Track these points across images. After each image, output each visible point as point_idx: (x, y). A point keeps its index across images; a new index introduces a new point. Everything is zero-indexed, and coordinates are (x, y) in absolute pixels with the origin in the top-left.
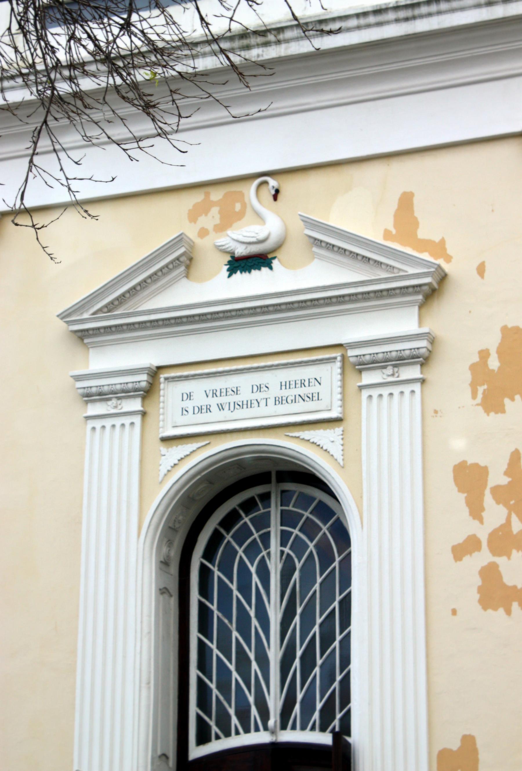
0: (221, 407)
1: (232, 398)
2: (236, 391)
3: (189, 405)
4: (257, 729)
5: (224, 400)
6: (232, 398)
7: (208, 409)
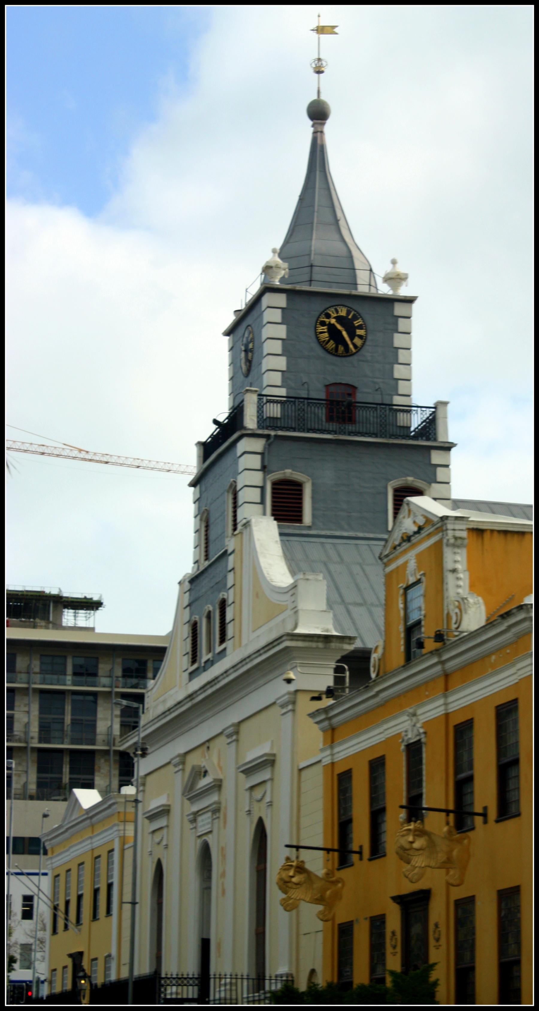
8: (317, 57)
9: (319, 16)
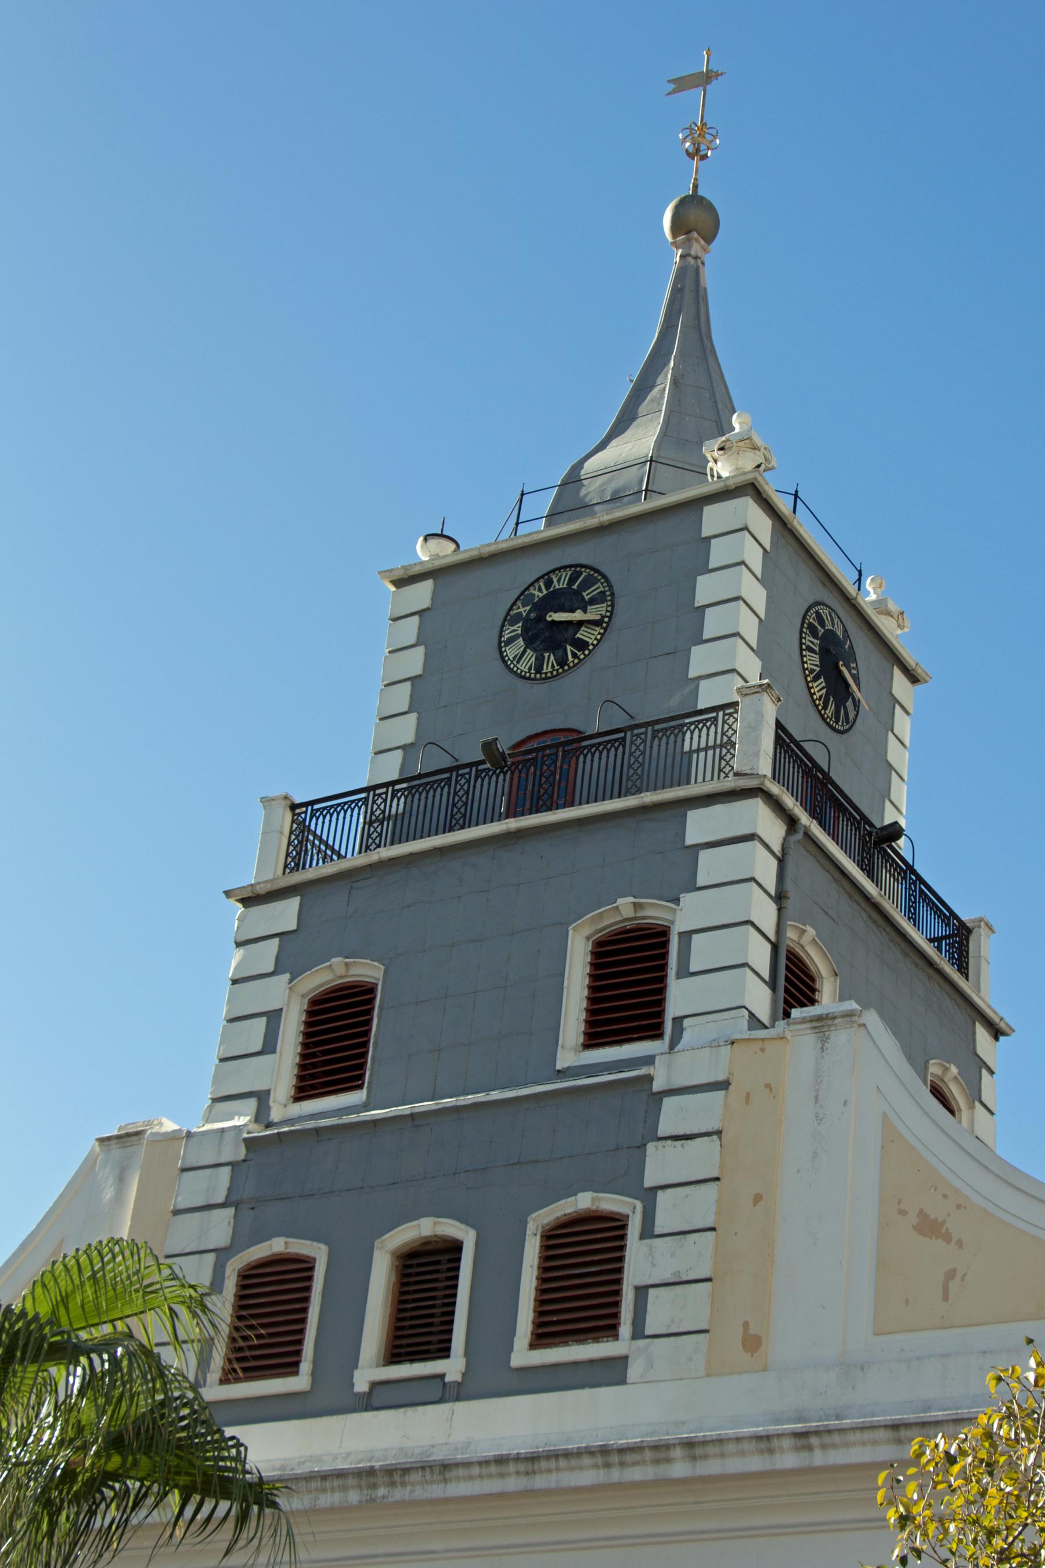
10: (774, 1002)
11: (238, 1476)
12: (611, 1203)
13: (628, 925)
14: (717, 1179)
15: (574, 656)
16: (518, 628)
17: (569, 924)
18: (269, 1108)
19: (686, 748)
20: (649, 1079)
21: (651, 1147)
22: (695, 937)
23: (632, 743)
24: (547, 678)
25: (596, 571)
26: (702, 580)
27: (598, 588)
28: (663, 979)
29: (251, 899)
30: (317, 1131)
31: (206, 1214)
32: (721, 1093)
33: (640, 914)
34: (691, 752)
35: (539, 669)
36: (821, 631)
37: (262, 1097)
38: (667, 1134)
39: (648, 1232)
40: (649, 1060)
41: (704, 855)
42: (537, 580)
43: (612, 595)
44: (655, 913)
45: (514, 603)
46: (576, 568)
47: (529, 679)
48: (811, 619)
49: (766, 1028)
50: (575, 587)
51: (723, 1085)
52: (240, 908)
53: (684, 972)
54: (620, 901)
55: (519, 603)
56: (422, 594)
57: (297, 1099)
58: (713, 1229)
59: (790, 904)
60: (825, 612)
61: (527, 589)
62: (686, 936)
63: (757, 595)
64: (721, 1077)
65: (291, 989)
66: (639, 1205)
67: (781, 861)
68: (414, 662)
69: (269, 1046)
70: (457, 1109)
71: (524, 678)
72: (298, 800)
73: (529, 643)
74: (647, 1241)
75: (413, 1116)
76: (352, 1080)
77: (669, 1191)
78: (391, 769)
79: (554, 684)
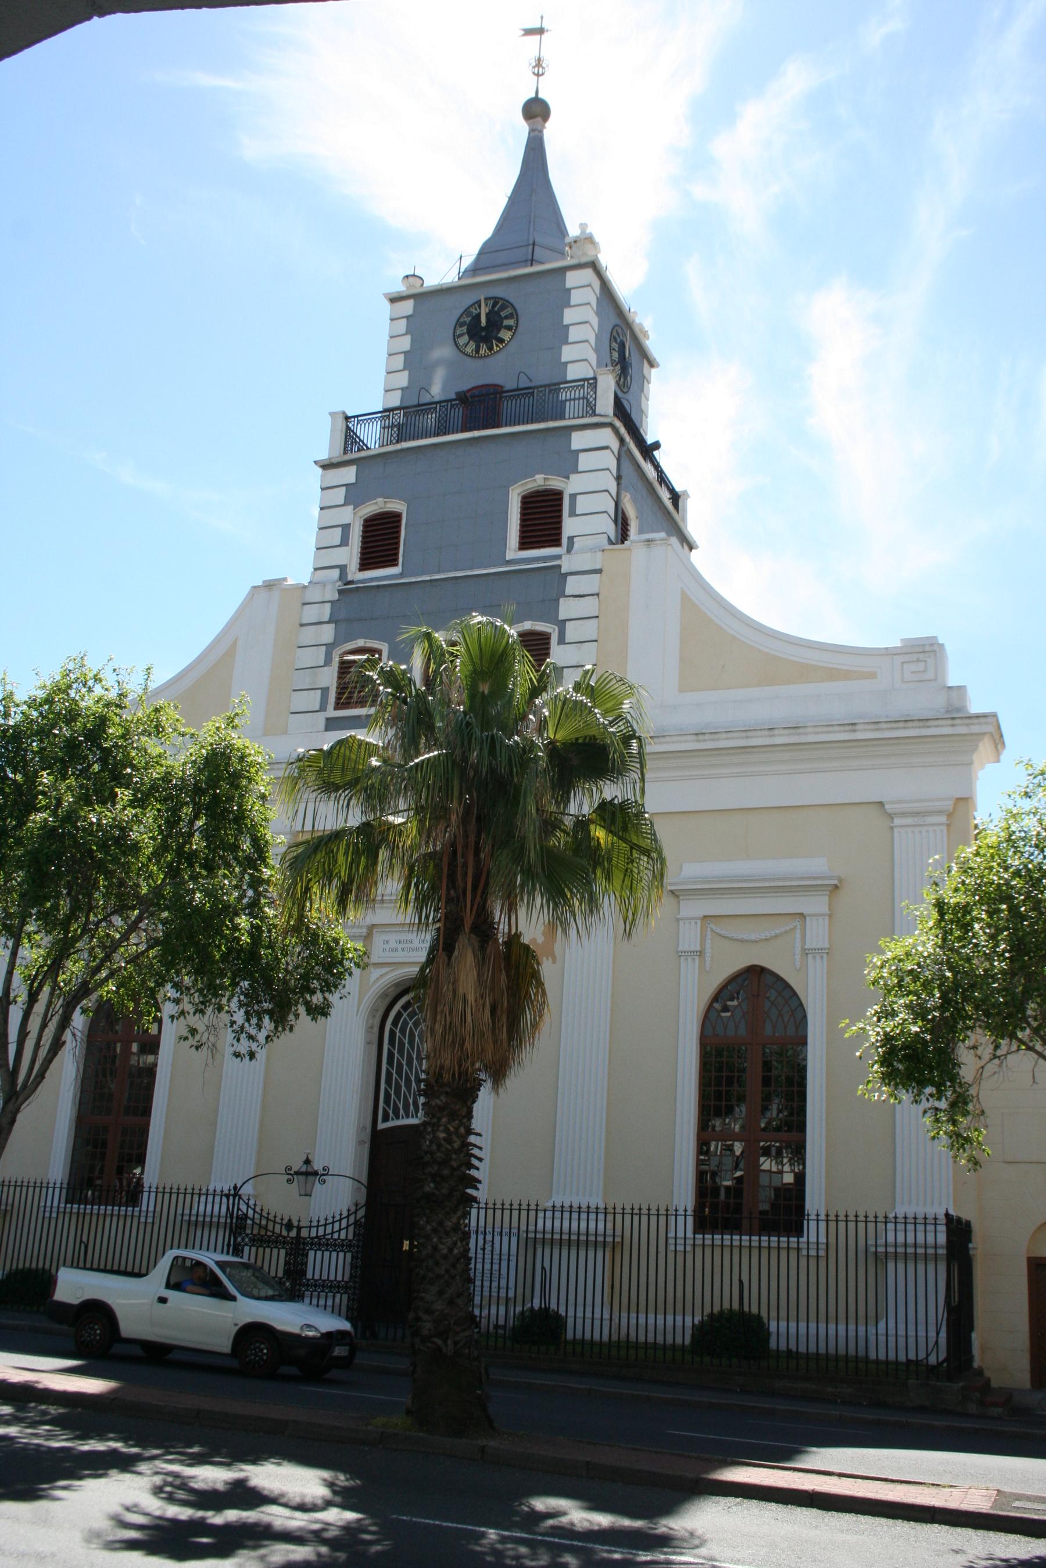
0: (403, 949)
1: (409, 945)
2: (411, 942)
3: (387, 946)
4: (413, 1117)
5: (405, 946)
6: (409, 945)
7: (396, 950)
8: (540, 78)
9: (542, 18)
10: (617, 531)
11: (1033, 1005)
12: (541, 627)
13: (540, 488)
14: (597, 617)
15: (497, 346)
16: (464, 329)
17: (509, 487)
18: (347, 574)
19: (564, 398)
20: (560, 567)
21: (562, 600)
22: (578, 496)
23: (538, 395)
24: (481, 357)
25: (507, 301)
26: (404, 383)
27: (509, 310)
28: (560, 517)
29: (326, 466)
30: (378, 587)
31: (319, 626)
32: (598, 575)
33: (547, 483)
34: (566, 400)
35: (477, 351)
36: (618, 340)
37: (343, 569)
38: (570, 594)
39: (562, 641)
40: (559, 557)
41: (581, 456)
42: (474, 304)
43: (517, 315)
44: (555, 483)
45: (461, 315)
46: (496, 300)
47: (472, 356)
48: (615, 333)
49: (614, 544)
50: (496, 309)
51: (599, 571)
52: (320, 471)
53: (573, 513)
54: (537, 476)
55: (464, 316)
56: (408, 307)
57: (361, 570)
58: (596, 641)
59: (623, 481)
60: (620, 331)
61: (469, 308)
62: (573, 497)
63: (595, 321)
64: (598, 567)
65: (354, 514)
66: (557, 628)
67: (619, 460)
68: (405, 343)
69: (344, 542)
70: (456, 578)
71: (469, 356)
72: (350, 414)
73: (471, 337)
74: (562, 646)
75: (431, 581)
76: (391, 560)
77: (572, 622)
78: (395, 400)
79: (488, 360)
